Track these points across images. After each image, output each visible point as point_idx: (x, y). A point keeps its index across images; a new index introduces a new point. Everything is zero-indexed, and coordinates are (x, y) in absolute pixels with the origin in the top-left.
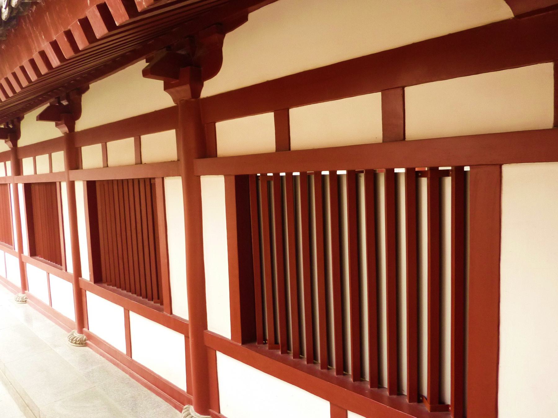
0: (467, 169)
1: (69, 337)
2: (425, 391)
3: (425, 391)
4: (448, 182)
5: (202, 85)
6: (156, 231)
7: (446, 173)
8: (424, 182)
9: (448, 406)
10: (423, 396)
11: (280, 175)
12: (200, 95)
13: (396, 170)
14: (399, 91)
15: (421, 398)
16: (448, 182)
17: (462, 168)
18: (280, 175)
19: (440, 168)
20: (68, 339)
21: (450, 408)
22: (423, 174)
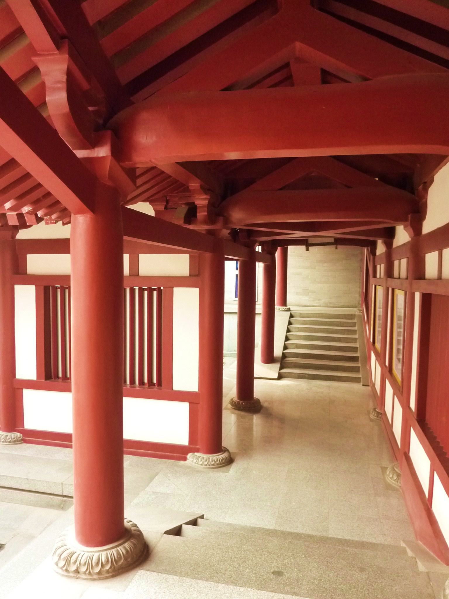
0: (162, 288)
1: (54, 553)
2: (146, 381)
3: (146, 381)
4: (155, 293)
5: (18, 232)
6: (399, 271)
7: (154, 289)
8: (146, 293)
9: (155, 383)
10: (145, 383)
11: (227, 263)
12: (15, 237)
13: (134, 287)
14: (137, 255)
15: (144, 384)
16: (155, 293)
17: (161, 288)
18: (227, 263)
19: (152, 288)
20: (56, 558)
21: (156, 384)
22: (154, 289)
